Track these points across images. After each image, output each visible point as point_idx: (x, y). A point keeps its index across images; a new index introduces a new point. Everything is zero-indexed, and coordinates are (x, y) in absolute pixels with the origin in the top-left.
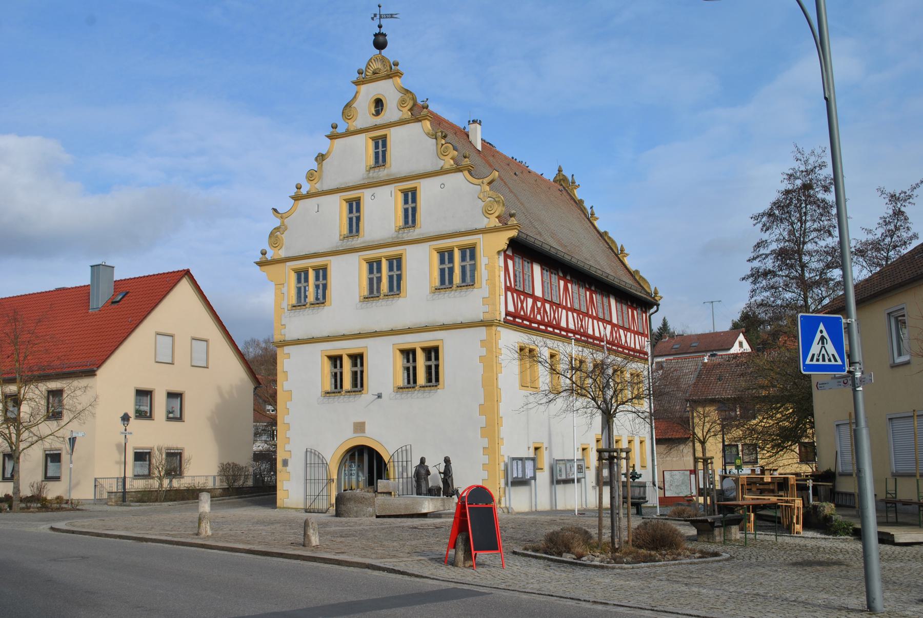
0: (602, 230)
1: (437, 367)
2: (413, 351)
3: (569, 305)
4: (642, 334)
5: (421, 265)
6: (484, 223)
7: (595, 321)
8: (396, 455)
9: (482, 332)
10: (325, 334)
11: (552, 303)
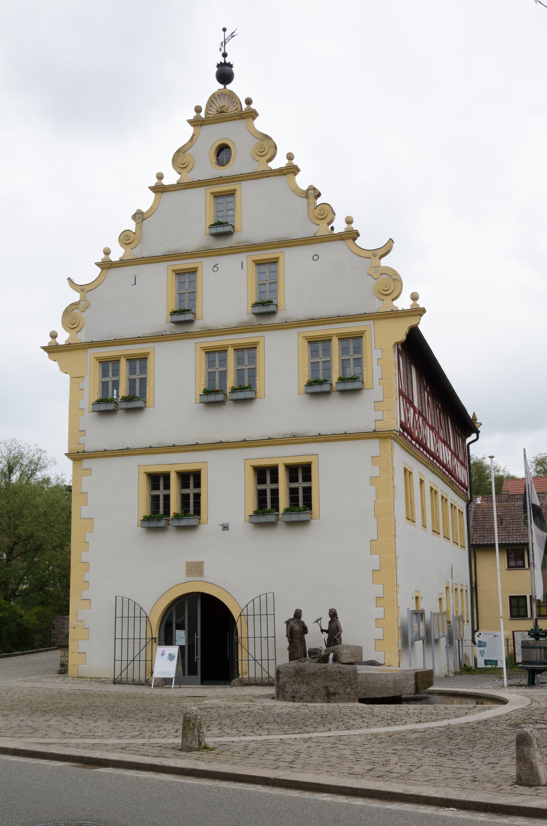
1: (197, 496)
2: (166, 476)
5: (282, 361)
8: (250, 606)
10: (146, 444)
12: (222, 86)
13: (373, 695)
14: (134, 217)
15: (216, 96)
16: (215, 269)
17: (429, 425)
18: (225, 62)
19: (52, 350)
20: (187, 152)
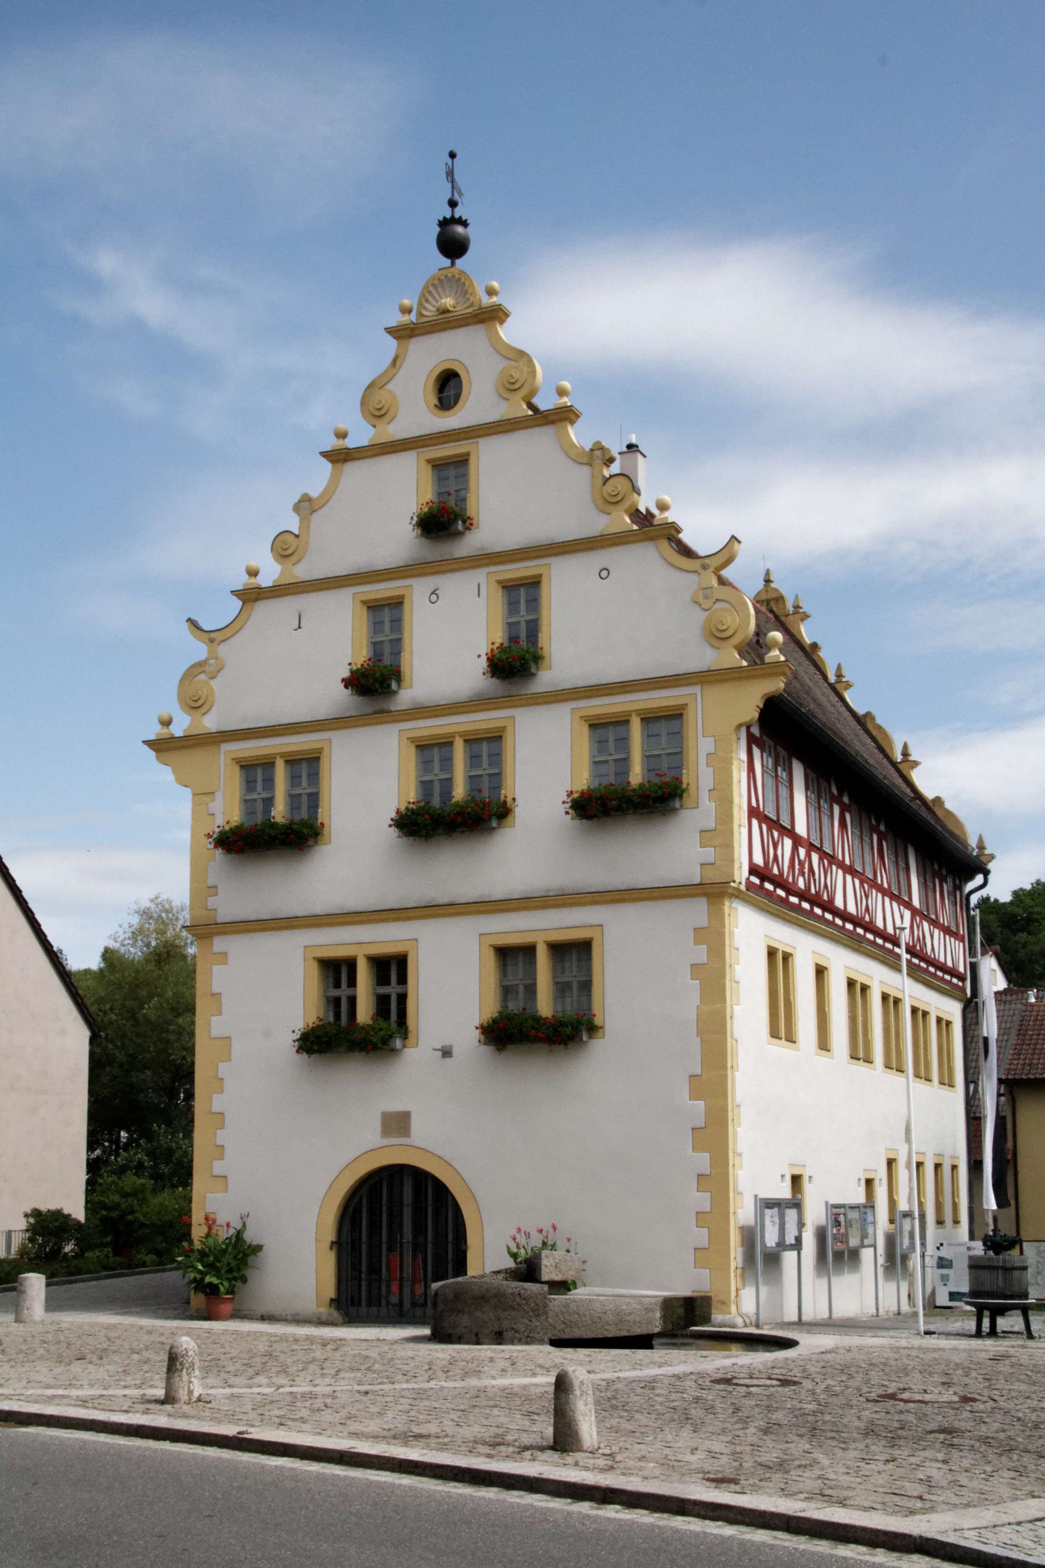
0: (861, 711)
1: (403, 998)
2: (351, 964)
3: (847, 862)
4: (955, 935)
6: (706, 658)
7: (887, 900)
9: (697, 911)
11: (823, 855)
12: (447, 262)
13: (577, 1333)
14: (297, 508)
15: (436, 282)
16: (434, 598)
17: (841, 865)
18: (453, 216)
19: (163, 746)
20: (386, 387)
